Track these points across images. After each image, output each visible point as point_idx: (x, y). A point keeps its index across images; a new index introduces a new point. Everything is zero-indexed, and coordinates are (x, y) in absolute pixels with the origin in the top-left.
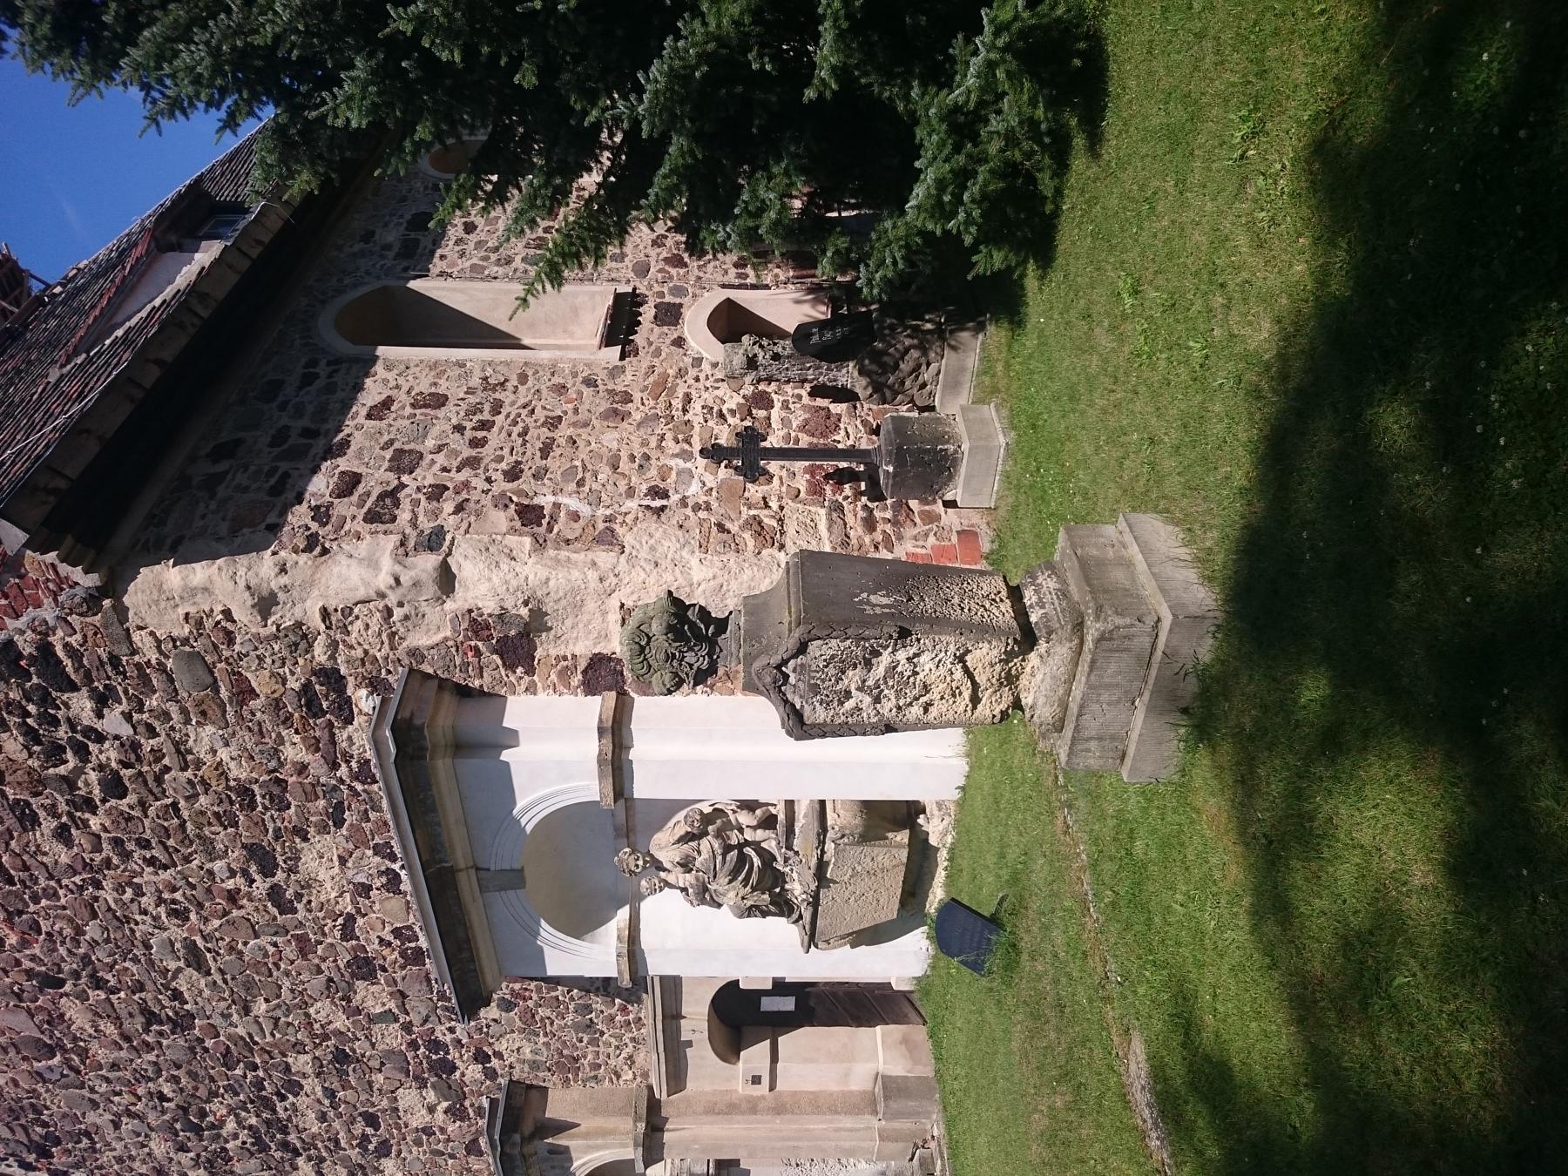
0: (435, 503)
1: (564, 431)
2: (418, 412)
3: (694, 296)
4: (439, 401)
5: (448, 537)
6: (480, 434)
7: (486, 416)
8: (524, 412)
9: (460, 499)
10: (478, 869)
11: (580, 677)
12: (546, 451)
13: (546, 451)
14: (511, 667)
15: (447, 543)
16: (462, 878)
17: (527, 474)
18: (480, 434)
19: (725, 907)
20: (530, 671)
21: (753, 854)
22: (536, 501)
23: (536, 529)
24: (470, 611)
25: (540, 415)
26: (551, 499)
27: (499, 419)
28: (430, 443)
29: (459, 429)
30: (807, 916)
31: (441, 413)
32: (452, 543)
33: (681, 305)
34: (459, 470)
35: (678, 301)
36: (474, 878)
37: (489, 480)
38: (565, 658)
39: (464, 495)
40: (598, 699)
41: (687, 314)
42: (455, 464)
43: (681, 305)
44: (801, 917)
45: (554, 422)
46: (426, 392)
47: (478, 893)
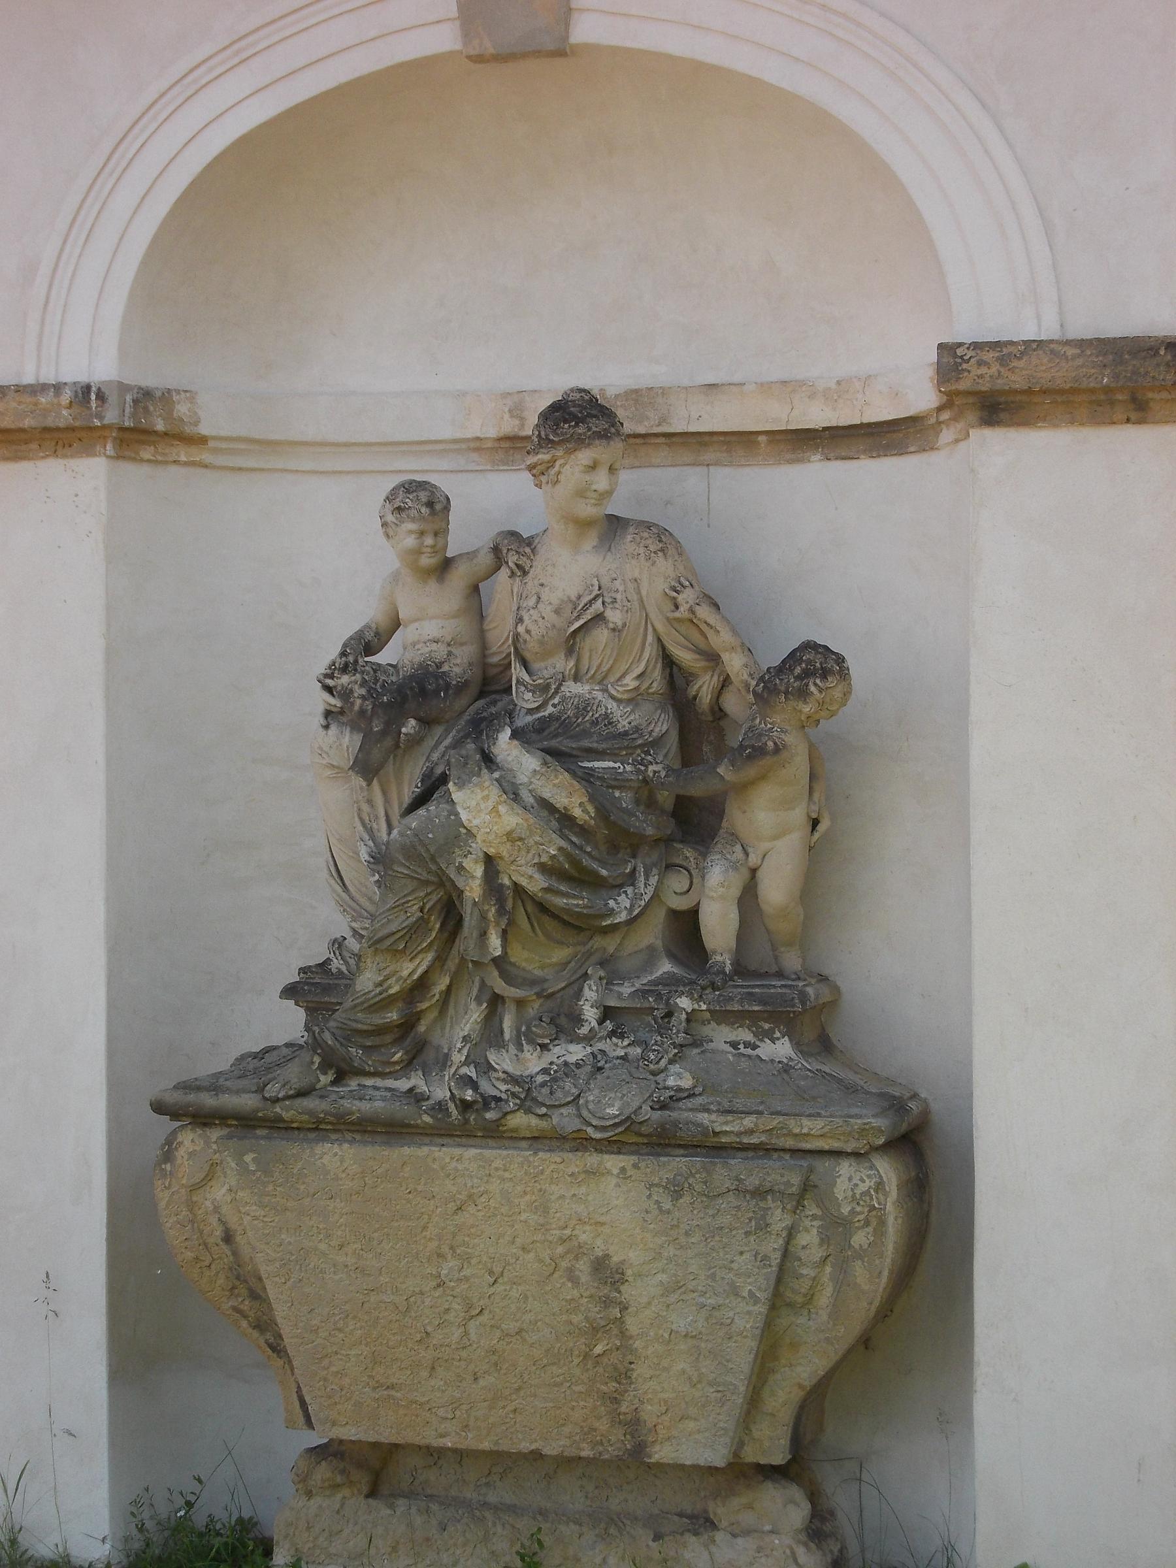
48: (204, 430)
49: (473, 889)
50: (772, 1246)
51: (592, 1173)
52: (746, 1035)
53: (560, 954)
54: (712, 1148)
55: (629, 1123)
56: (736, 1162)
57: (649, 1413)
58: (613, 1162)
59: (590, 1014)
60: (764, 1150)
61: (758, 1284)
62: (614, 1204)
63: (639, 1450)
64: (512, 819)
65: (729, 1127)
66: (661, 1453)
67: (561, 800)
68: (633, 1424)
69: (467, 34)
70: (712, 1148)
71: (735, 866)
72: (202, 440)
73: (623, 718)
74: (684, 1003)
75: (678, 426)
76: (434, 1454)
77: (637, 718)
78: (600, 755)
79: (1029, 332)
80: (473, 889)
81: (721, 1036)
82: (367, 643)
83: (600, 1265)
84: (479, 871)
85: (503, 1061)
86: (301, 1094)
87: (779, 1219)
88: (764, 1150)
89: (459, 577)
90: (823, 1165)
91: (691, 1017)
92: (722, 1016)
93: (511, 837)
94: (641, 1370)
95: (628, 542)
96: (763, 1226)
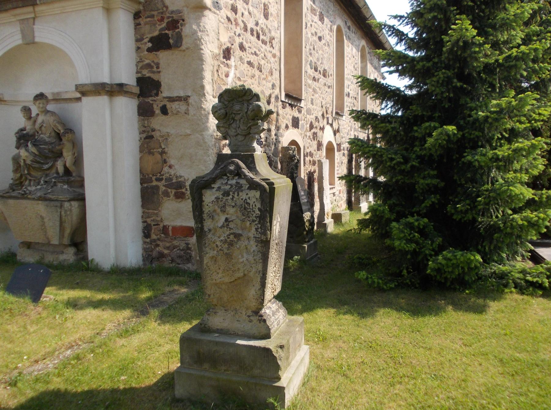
0: (230, 8)
1: (257, 73)
2: (262, 5)
3: (301, 134)
4: (266, 16)
5: (218, 12)
6: (255, 33)
7: (261, 37)
8: (263, 55)
9: (233, 20)
10: (34, 19)
11: (148, 75)
12: (249, 63)
13: (249, 63)
14: (151, 40)
15: (216, 11)
16: (30, 9)
17: (241, 54)
18: (255, 33)
19: (17, 151)
20: (149, 50)
21: (50, 164)
22: (232, 58)
23: (222, 56)
24: (183, 20)
25: (262, 62)
26: (233, 64)
27: (260, 42)
28: (251, 9)
29: (257, 24)
30: (14, 194)
31: (262, 16)
32: (215, 13)
33: (298, 128)
34: (243, 21)
35: (300, 127)
36: (29, 16)
37: (239, 35)
38: (158, 68)
39: (234, 23)
40: (135, 83)
41: (296, 130)
42: (244, 20)
43: (298, 128)
44: (14, 190)
45: (260, 69)
46: (269, 10)
47: (19, 18)
48: (5, 99)
49: (22, 164)
50: (59, 214)
51: (38, 204)
52: (62, 185)
53: (41, 173)
54: (51, 200)
55: (40, 197)
56: (53, 202)
57: (49, 237)
58: (40, 202)
59: (42, 182)
60: (57, 200)
61: (58, 219)
62: (41, 208)
63: (49, 242)
64: (26, 154)
65: (52, 197)
66: (52, 243)
67: (34, 151)
68: (48, 238)
69: (23, 40)
70: (51, 200)
71: (62, 161)
72: (5, 101)
73: (47, 140)
74: (53, 180)
75: (62, 98)
76: (36, 243)
77: (49, 140)
78: (41, 145)
79: (87, 83)
80: (22, 164)
81: (59, 185)
82: (22, 130)
83: (41, 216)
84: (22, 161)
85: (29, 188)
86: (7, 193)
87: (59, 210)
88: (57, 200)
89: (32, 120)
90: (63, 203)
91: (55, 182)
92: (59, 182)
93: (26, 156)
94: (48, 231)
95: (48, 115)
96: (57, 212)
